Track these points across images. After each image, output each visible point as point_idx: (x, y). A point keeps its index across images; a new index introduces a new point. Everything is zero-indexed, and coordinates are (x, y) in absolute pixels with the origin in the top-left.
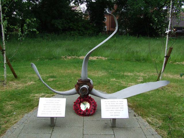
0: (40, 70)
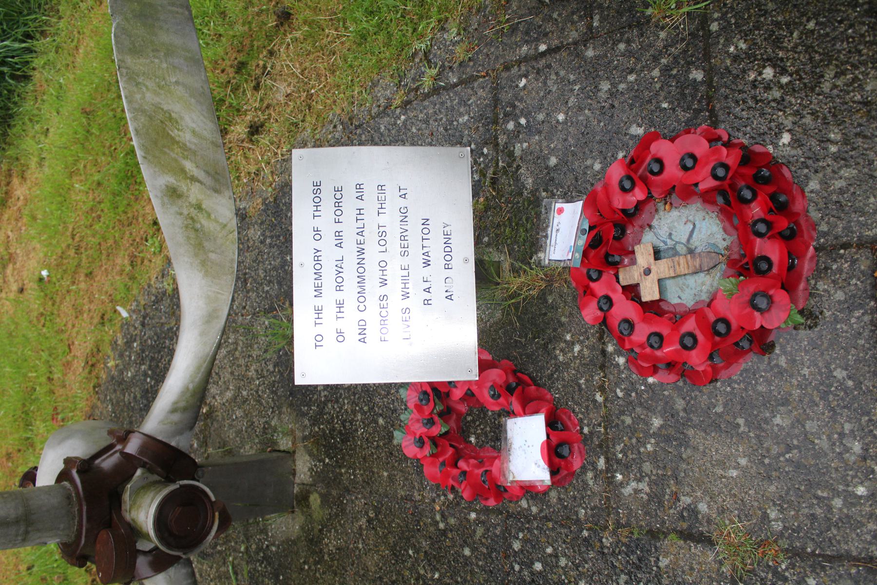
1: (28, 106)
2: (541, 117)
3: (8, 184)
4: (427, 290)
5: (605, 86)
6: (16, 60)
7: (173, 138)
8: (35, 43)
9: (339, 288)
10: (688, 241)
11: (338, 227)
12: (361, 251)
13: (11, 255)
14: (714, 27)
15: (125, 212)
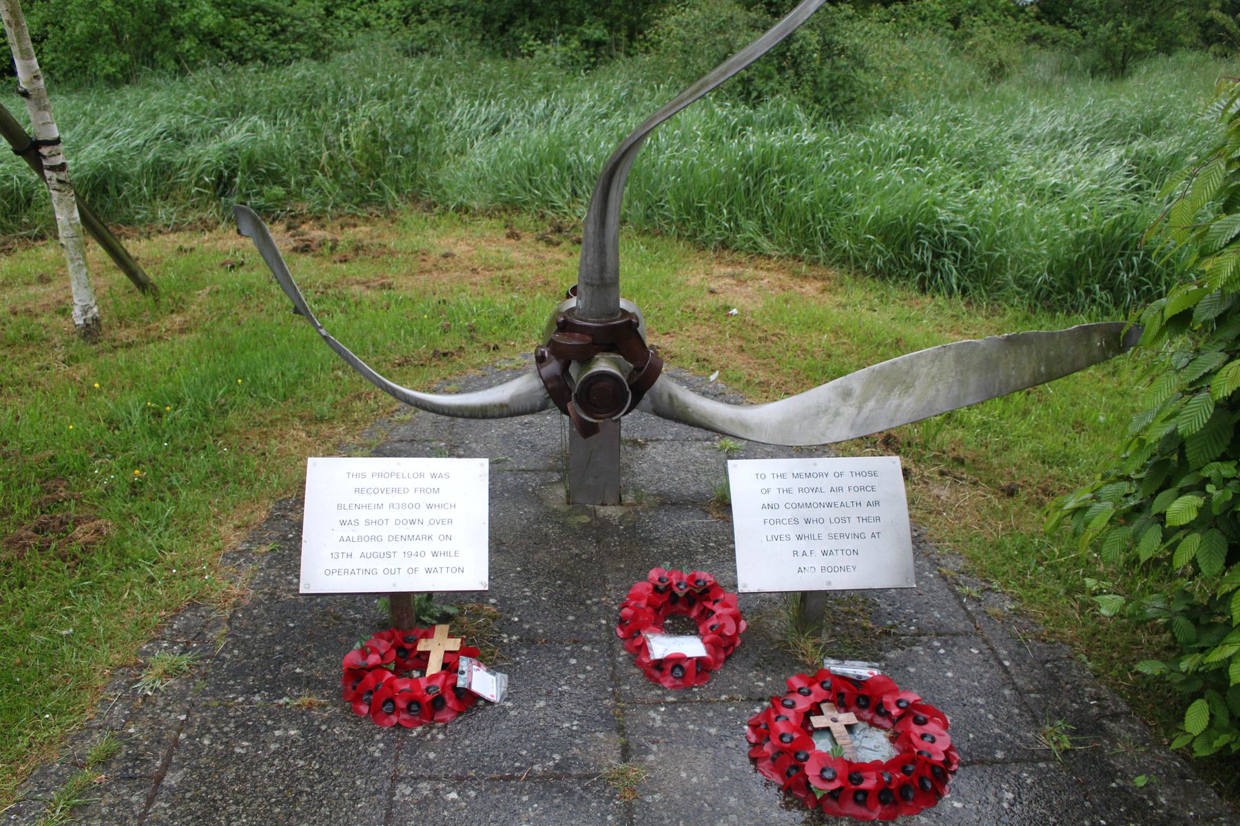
0: (50, 213)
1: (896, 293)
2: (947, 662)
3: (815, 278)
4: (804, 554)
5: (980, 701)
6: (939, 281)
7: (892, 390)
8: (959, 297)
9: (801, 490)
10: (864, 747)
11: (846, 489)
12: (829, 505)
13: (746, 281)
14: (1042, 765)
15: (808, 377)
